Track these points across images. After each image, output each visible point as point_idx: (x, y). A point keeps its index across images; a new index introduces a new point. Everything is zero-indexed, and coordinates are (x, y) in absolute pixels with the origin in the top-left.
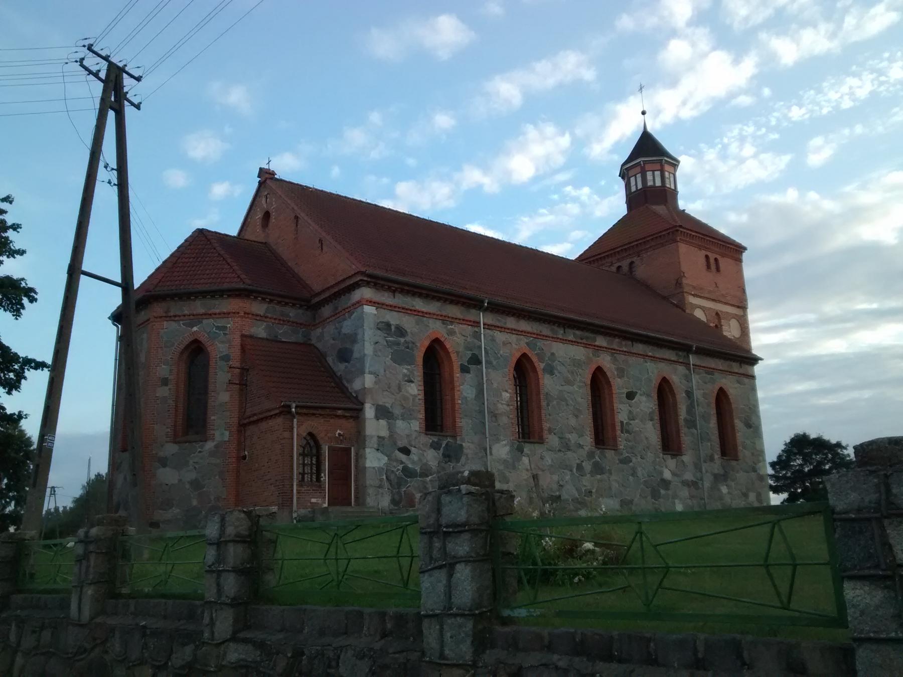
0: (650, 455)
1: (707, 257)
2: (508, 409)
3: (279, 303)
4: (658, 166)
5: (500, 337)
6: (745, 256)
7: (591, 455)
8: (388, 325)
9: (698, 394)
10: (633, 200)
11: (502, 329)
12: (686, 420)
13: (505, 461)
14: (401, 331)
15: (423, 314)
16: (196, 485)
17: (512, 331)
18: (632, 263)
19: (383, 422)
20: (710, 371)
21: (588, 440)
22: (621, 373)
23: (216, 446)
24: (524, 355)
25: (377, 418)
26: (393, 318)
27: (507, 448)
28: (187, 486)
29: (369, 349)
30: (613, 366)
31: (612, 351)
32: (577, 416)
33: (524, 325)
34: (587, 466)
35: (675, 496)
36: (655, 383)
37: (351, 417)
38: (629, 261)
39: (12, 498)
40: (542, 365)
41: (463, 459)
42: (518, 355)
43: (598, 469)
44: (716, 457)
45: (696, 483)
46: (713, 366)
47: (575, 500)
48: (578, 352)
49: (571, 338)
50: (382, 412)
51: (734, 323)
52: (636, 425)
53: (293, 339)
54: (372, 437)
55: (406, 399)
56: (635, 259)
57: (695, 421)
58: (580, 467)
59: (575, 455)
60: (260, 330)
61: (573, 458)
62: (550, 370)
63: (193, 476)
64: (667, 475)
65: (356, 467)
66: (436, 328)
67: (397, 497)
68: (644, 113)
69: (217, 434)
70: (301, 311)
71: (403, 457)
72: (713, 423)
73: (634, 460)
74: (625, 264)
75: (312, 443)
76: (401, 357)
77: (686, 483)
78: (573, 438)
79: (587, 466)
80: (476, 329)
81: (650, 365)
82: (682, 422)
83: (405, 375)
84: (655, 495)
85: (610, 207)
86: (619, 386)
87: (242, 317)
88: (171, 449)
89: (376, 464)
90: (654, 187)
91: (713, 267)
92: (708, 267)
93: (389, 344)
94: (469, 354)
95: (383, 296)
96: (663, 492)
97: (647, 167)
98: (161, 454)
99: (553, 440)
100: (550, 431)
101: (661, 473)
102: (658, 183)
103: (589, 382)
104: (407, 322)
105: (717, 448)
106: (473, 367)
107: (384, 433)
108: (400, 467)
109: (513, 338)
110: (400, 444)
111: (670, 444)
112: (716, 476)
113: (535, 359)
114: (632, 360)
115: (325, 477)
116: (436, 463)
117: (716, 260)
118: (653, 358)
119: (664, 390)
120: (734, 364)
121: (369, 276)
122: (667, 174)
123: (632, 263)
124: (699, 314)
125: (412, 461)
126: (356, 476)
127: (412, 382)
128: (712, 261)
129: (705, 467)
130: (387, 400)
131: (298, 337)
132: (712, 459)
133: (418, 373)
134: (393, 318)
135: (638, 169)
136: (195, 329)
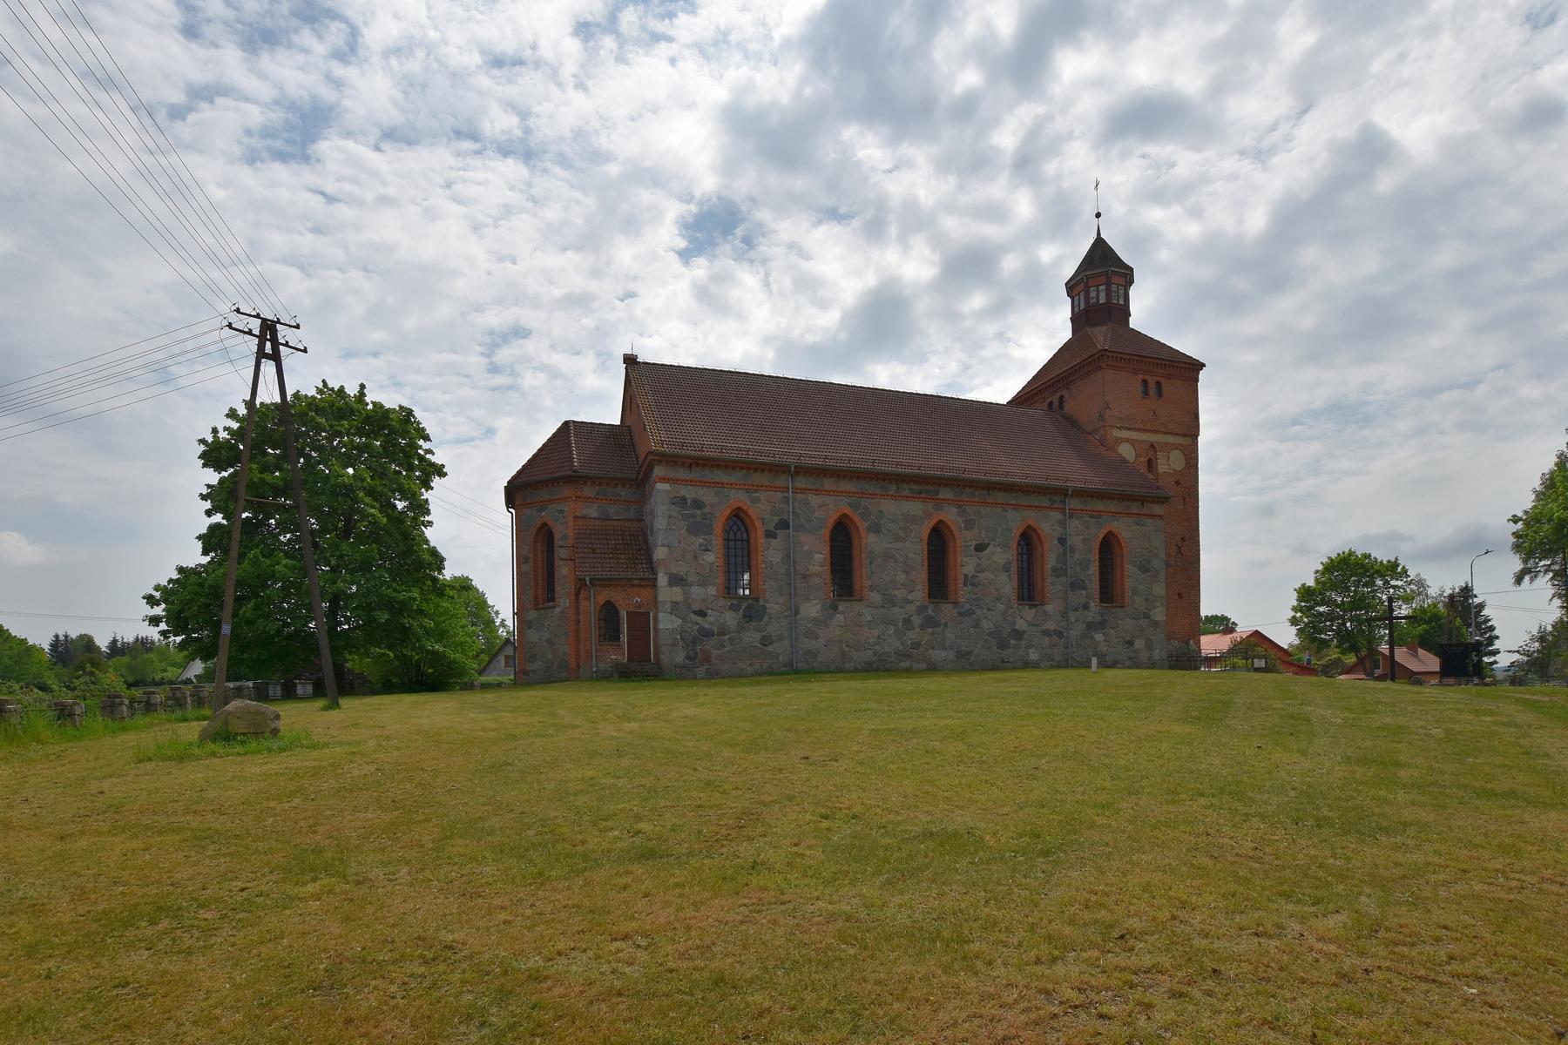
1: (1145, 382)
5: (814, 500)
8: (684, 499)
9: (1075, 541)
11: (818, 492)
12: (1054, 569)
13: (815, 620)
14: (698, 504)
16: (550, 642)
17: (830, 492)
18: (1062, 397)
19: (677, 589)
20: (1096, 515)
21: (920, 594)
22: (969, 525)
24: (845, 515)
25: (670, 585)
26: (689, 492)
29: (660, 523)
32: (906, 572)
33: (846, 486)
34: (916, 620)
36: (1016, 533)
40: (866, 524)
41: (766, 618)
42: (836, 516)
43: (930, 622)
48: (916, 507)
49: (906, 493)
50: (676, 580)
58: (907, 622)
60: (592, 511)
61: (898, 613)
63: (547, 636)
64: (1021, 625)
66: (738, 498)
71: (699, 619)
72: (1094, 570)
73: (979, 612)
74: (1055, 399)
76: (699, 527)
77: (1046, 633)
78: (900, 594)
79: (916, 620)
81: (1011, 514)
82: (1048, 571)
84: (1003, 645)
85: (1043, 333)
86: (964, 539)
89: (669, 626)
90: (1097, 304)
92: (1146, 393)
93: (685, 517)
94: (776, 520)
100: (872, 589)
101: (1014, 624)
103: (926, 537)
104: (707, 496)
105: (1097, 596)
106: (780, 533)
107: (679, 598)
109: (830, 500)
110: (696, 607)
111: (1029, 592)
113: (857, 519)
115: (624, 638)
117: (1158, 383)
118: (1016, 507)
119: (1028, 541)
123: (1062, 397)
124: (1127, 451)
128: (1152, 385)
129: (1072, 616)
130: (680, 569)
132: (1086, 607)
134: (689, 492)
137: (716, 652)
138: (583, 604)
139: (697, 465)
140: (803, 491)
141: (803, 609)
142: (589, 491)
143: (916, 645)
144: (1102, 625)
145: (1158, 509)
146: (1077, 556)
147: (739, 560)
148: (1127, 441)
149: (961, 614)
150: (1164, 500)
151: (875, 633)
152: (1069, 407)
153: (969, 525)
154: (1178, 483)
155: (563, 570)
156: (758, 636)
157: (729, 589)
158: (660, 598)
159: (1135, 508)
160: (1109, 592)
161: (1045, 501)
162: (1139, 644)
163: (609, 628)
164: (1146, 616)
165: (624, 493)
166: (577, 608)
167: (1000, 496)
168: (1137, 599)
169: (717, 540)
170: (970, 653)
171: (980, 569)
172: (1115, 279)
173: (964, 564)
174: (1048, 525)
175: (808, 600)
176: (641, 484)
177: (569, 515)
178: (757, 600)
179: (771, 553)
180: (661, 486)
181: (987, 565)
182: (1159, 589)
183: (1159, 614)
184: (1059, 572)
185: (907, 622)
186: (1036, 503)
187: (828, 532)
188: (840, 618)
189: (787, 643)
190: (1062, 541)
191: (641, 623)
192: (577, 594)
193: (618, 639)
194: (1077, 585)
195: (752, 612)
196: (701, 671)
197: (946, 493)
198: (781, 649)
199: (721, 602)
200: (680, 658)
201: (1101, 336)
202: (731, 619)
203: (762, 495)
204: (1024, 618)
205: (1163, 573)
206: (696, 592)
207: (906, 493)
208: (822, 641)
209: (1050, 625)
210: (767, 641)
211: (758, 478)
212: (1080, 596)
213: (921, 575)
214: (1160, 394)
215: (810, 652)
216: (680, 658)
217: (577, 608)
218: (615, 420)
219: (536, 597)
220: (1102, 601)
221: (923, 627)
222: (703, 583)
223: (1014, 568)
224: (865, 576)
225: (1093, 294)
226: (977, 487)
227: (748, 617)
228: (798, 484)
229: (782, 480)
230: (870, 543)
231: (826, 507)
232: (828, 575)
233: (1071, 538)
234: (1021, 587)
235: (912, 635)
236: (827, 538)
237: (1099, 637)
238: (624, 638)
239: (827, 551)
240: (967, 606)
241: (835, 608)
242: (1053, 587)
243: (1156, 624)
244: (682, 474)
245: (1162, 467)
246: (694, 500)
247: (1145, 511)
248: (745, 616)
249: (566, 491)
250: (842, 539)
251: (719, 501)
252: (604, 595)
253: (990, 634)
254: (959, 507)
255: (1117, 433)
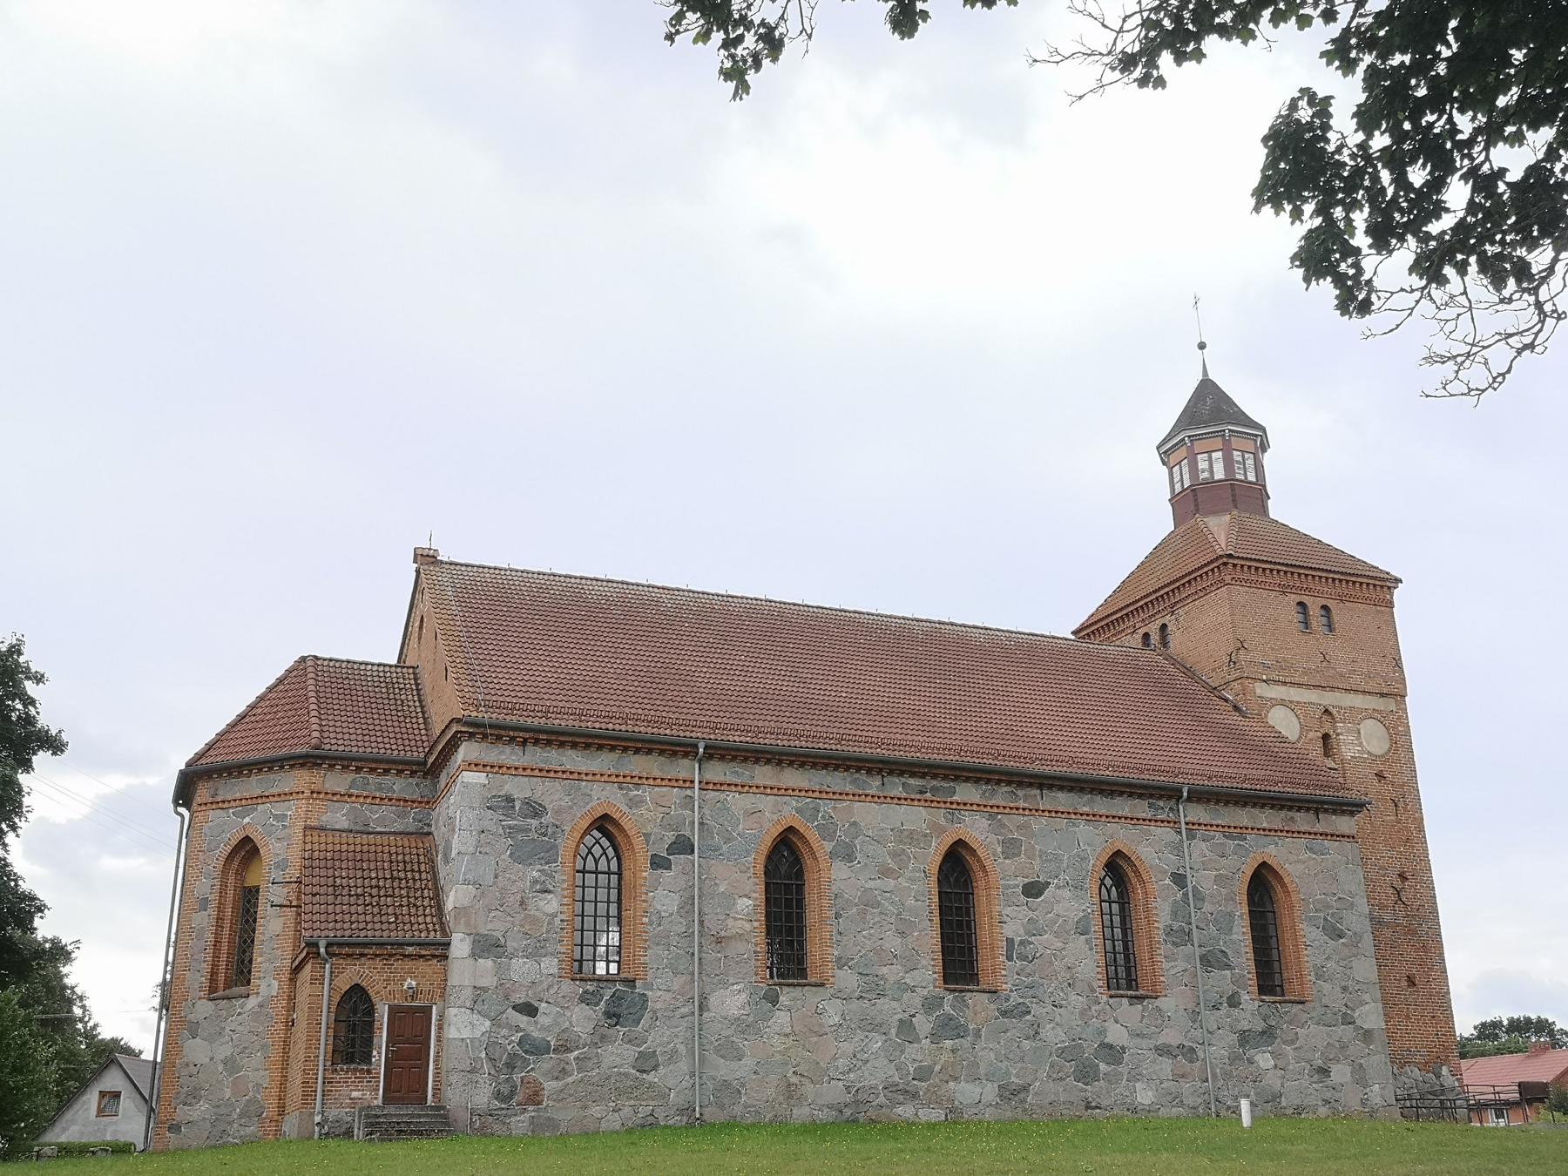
0: (1076, 1000)
2: (748, 926)
4: (1218, 443)
5: (452, 1033)
6: (1398, 595)
7: (931, 1004)
8: (509, 799)
9: (1204, 880)
10: (1191, 502)
12: (1169, 931)
14: (534, 809)
15: (578, 776)
16: (230, 1064)
17: (764, 790)
18: (1164, 626)
19: (486, 964)
20: (1238, 833)
21: (928, 972)
22: (1011, 848)
23: (261, 1006)
25: (474, 955)
26: (519, 788)
28: (221, 1068)
30: (992, 838)
31: (993, 812)
33: (793, 778)
34: (923, 1024)
35: (1135, 1077)
36: (1095, 861)
37: (434, 956)
38: (1159, 622)
40: (828, 846)
43: (948, 1028)
44: (1245, 997)
45: (1192, 1050)
46: (1245, 822)
47: (890, 1087)
48: (916, 817)
49: (898, 791)
50: (486, 947)
51: (1370, 728)
52: (1046, 942)
53: (398, 826)
55: (535, 921)
56: (1166, 620)
57: (1189, 934)
58: (906, 1027)
59: (895, 1004)
60: (338, 817)
61: (890, 1010)
62: (847, 854)
63: (224, 1051)
64: (1116, 1035)
65: (439, 1039)
67: (505, 1089)
68: (1202, 346)
70: (413, 781)
71: (522, 1020)
72: (1241, 933)
73: (1035, 1009)
74: (1153, 629)
75: (356, 1004)
77: (1163, 1051)
78: (891, 973)
79: (923, 1024)
80: (689, 792)
81: (1084, 830)
82: (1160, 936)
83: (536, 882)
84: (1086, 1074)
87: (308, 798)
90: (1211, 482)
91: (1317, 620)
92: (1306, 623)
93: (511, 832)
94: (670, 837)
95: (502, 752)
97: (1198, 446)
98: (191, 1017)
99: (847, 979)
100: (841, 963)
101: (1102, 1032)
102: (1219, 474)
104: (551, 794)
107: (488, 981)
108: (516, 1037)
109: (766, 803)
110: (520, 997)
111: (1125, 974)
112: (1245, 1038)
113: (812, 836)
114: (1038, 824)
115: (380, 1056)
116: (590, 1028)
118: (1092, 817)
120: (1298, 816)
121: (467, 724)
122: (1237, 455)
123: (1164, 626)
124: (1284, 722)
125: (541, 1028)
126: (437, 1055)
127: (550, 892)
128: (1314, 611)
130: (494, 926)
131: (409, 823)
132: (1233, 1001)
134: (519, 788)
136: (247, 820)
137: (550, 1086)
138: (305, 990)
139: (537, 742)
140: (719, 786)
141: (713, 1001)
142: (337, 781)
143: (923, 1074)
144: (1268, 1035)
145: (1344, 824)
146: (1207, 907)
147: (602, 907)
148: (1283, 703)
149: (1004, 1014)
150: (1351, 808)
151: (847, 1047)
152: (1178, 642)
153: (1011, 848)
154: (1380, 776)
155: (273, 928)
156: (631, 1052)
157: (578, 968)
158: (454, 980)
159: (1302, 821)
160: (1270, 975)
161: (1141, 808)
162: (1341, 1073)
163: (351, 1044)
164: (1348, 1021)
165: (399, 785)
166: (292, 998)
167: (1063, 799)
168: (1326, 987)
169: (562, 875)
170: (1025, 1089)
171: (1034, 929)
172: (1235, 442)
173: (1003, 917)
174: (1152, 848)
175: (725, 985)
176: (430, 768)
177: (285, 822)
178: (631, 982)
179: (661, 896)
180: (470, 777)
181: (1044, 917)
182: (1365, 969)
183: (1371, 1016)
184: (1181, 936)
185: (906, 1027)
186: (1126, 812)
187: (762, 860)
188: (781, 1018)
189: (683, 1066)
190: (1179, 879)
191: (414, 1027)
192: (297, 970)
193: (367, 1058)
194: (1211, 961)
195: (620, 1005)
196: (520, 1122)
197: (966, 792)
198: (672, 1078)
199: (567, 987)
200: (482, 1097)
201: (1220, 529)
202: (582, 1020)
203: (646, 793)
204: (1121, 1023)
205: (1368, 940)
206: (520, 968)
207: (898, 791)
208: (749, 1062)
209: (1171, 1037)
210: (647, 1063)
211: (638, 764)
212: (1222, 980)
213: (928, 938)
214: (1330, 626)
215: (726, 1084)
216: (482, 1097)
217: (292, 998)
218: (394, 661)
219: (213, 974)
220: (1262, 990)
221: (935, 1037)
222: (535, 954)
223: (1095, 927)
224: (824, 940)
225: (1203, 464)
226: (1020, 784)
227: (614, 1016)
228: (709, 776)
229: (685, 768)
230: (833, 881)
231: (754, 812)
232: (760, 938)
233: (1187, 869)
234: (1110, 963)
235: (917, 1054)
236: (761, 869)
237: (1264, 1060)
238: (380, 1056)
239: (759, 895)
240: (1015, 999)
241: (774, 1001)
242: (1170, 965)
243: (1367, 1035)
244: (509, 755)
245: (1348, 748)
246: (527, 803)
247: (1319, 828)
248: (608, 1015)
249: (299, 779)
250: (786, 870)
251: (573, 792)
252: (352, 973)
253: (1061, 1052)
254: (992, 817)
255: (1262, 690)
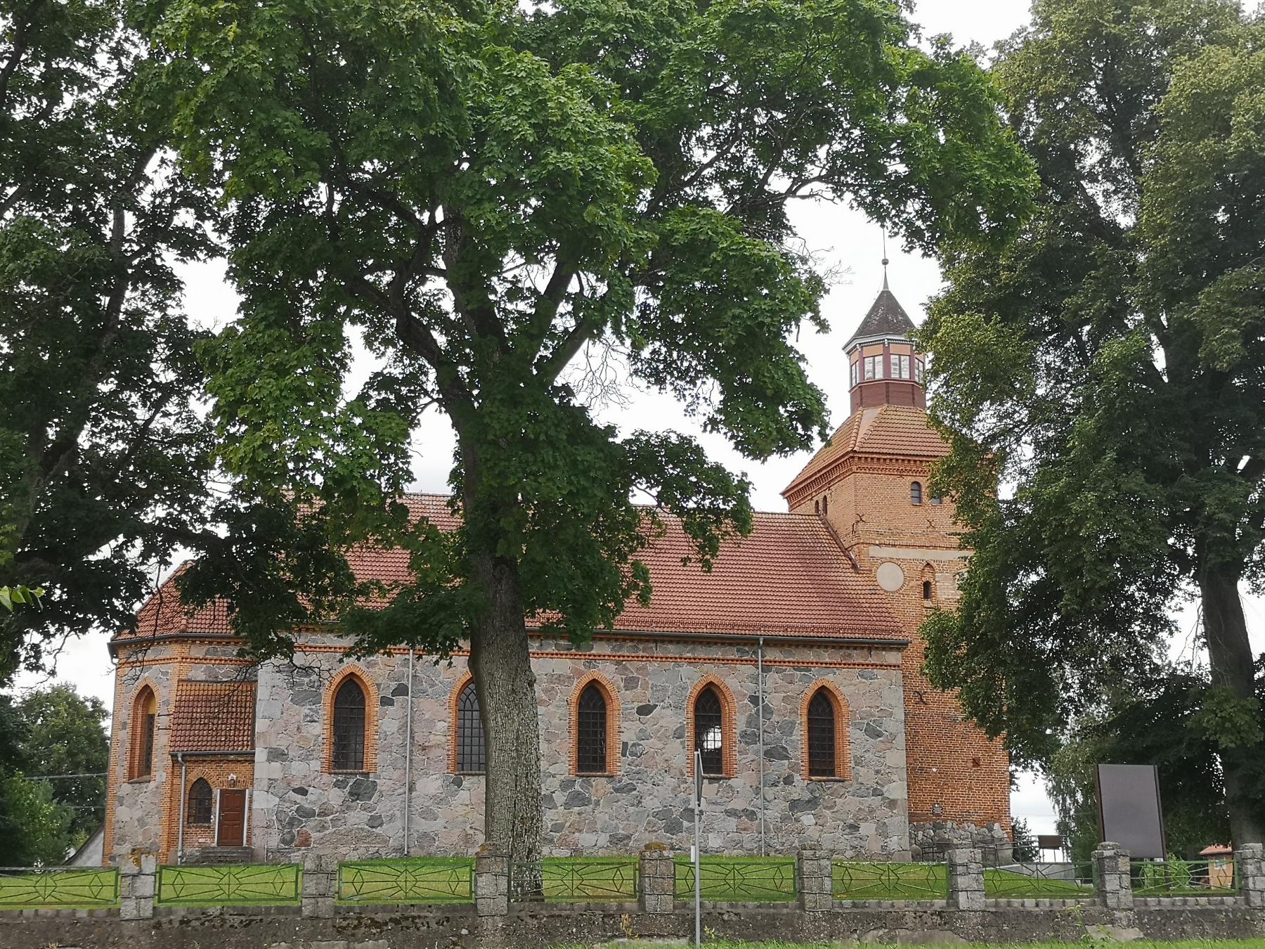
3: (219, 643)
19: (276, 765)
22: (630, 683)
27: (439, 782)
39: (1131, 665)
44: (797, 777)
49: (552, 649)
52: (651, 744)
54: (262, 779)
60: (199, 673)
67: (288, 837)
68: (885, 262)
69: (158, 774)
71: (298, 798)
83: (307, 716)
86: (622, 701)
88: (126, 788)
94: (394, 685)
96: (686, 824)
110: (296, 785)
125: (311, 801)
133: (325, 709)
135: (880, 349)
